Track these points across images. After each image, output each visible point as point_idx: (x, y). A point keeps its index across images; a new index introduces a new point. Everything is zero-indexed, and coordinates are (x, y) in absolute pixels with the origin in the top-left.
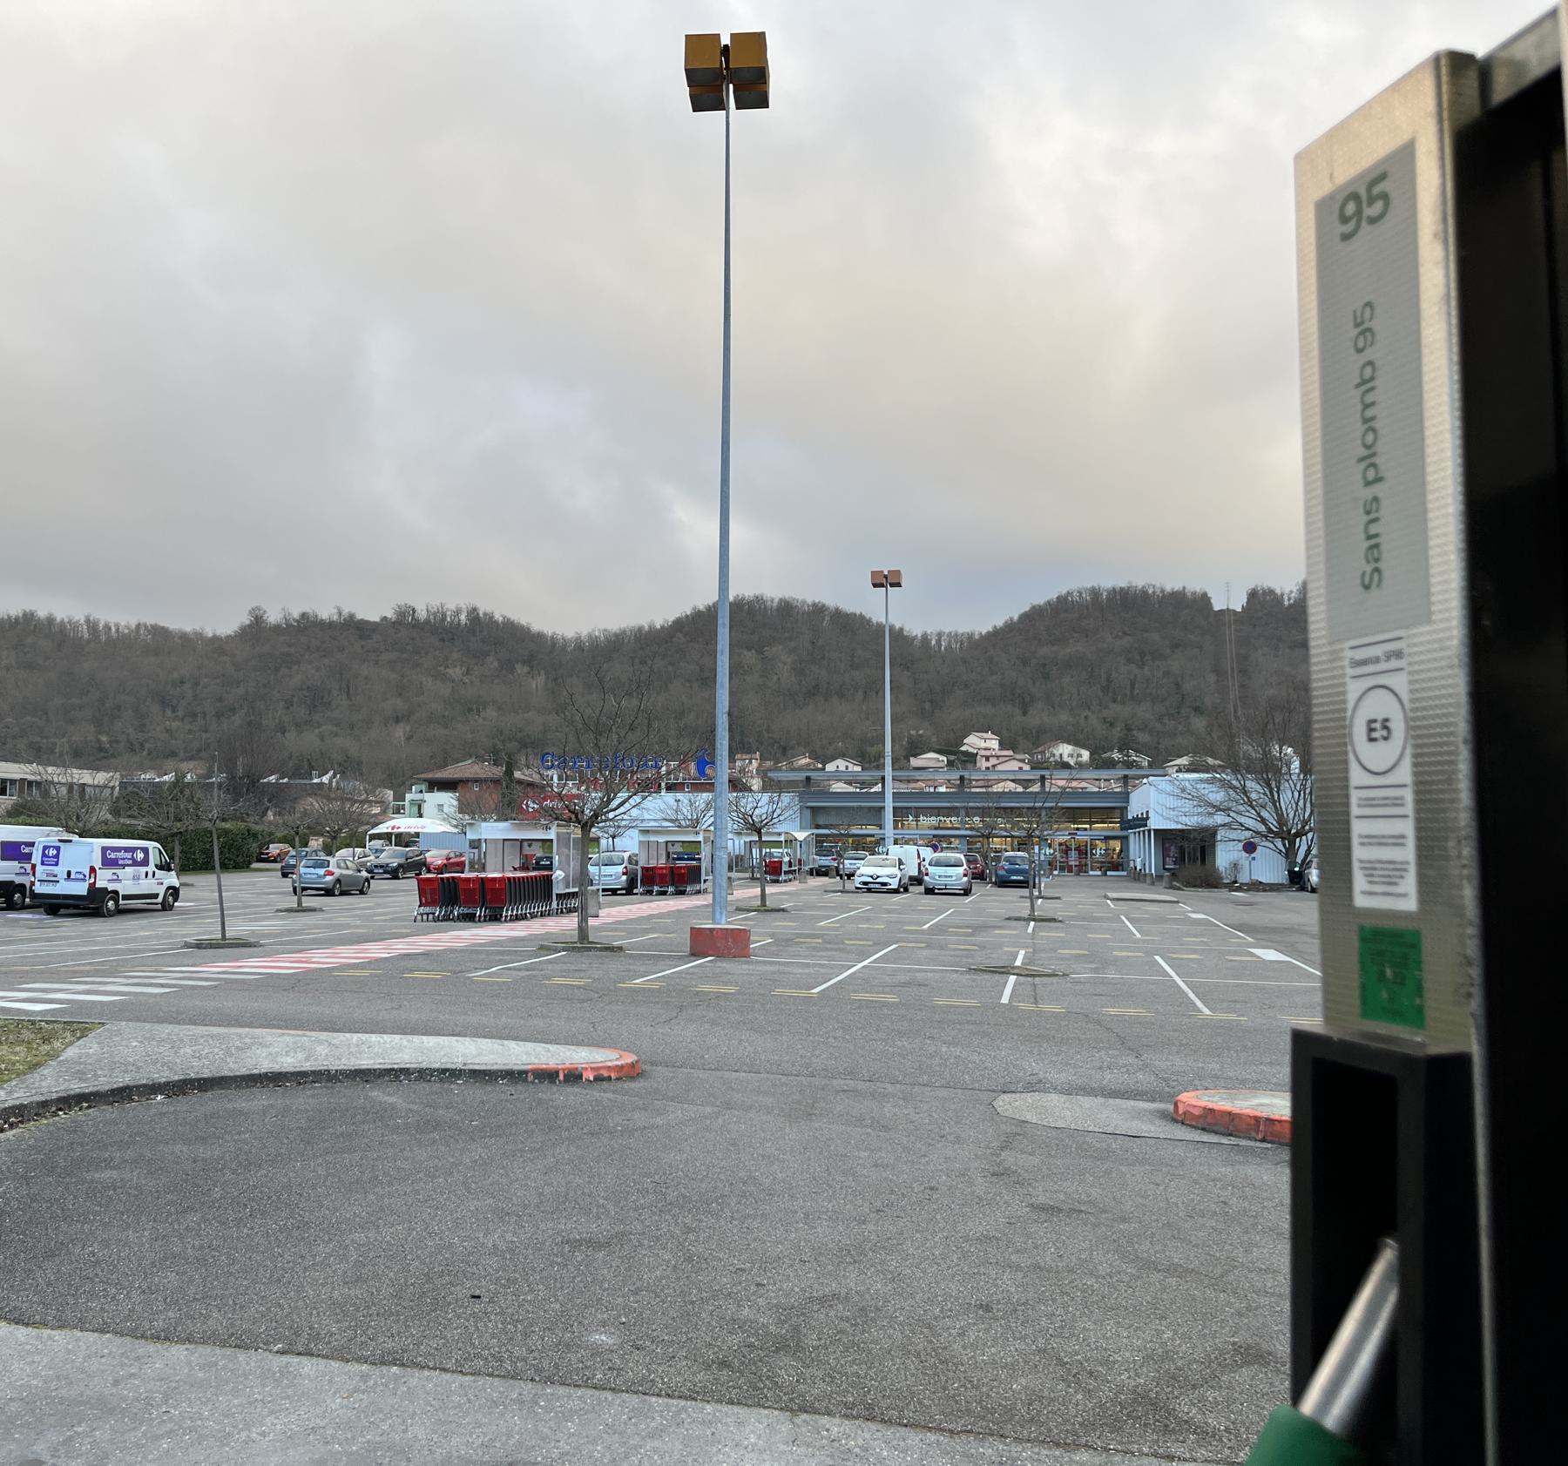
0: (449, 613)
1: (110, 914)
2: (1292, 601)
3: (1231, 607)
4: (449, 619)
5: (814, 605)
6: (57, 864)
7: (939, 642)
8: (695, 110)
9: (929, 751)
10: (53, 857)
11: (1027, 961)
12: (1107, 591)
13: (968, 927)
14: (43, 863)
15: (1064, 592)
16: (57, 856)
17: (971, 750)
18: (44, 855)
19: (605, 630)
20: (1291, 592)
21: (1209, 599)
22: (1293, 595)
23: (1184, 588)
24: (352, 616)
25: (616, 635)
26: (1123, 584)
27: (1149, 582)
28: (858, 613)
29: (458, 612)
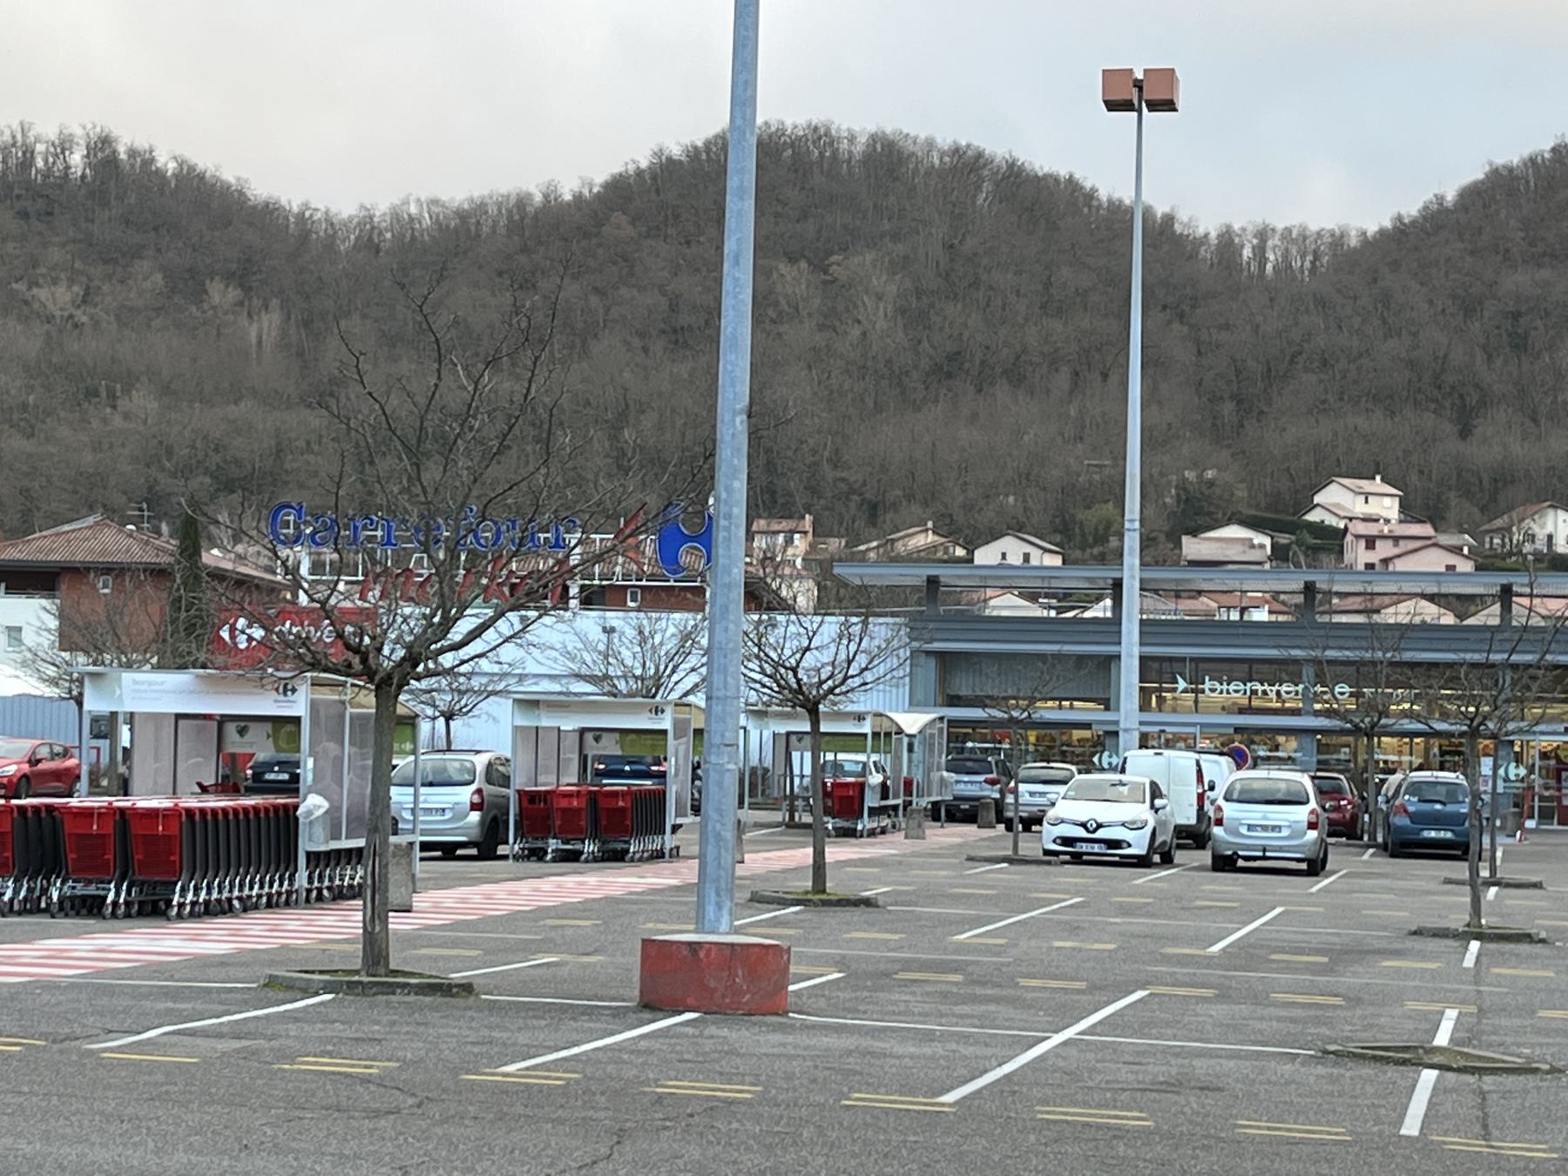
4: (40, 163)
5: (956, 151)
19: (435, 202)
29: (64, 145)
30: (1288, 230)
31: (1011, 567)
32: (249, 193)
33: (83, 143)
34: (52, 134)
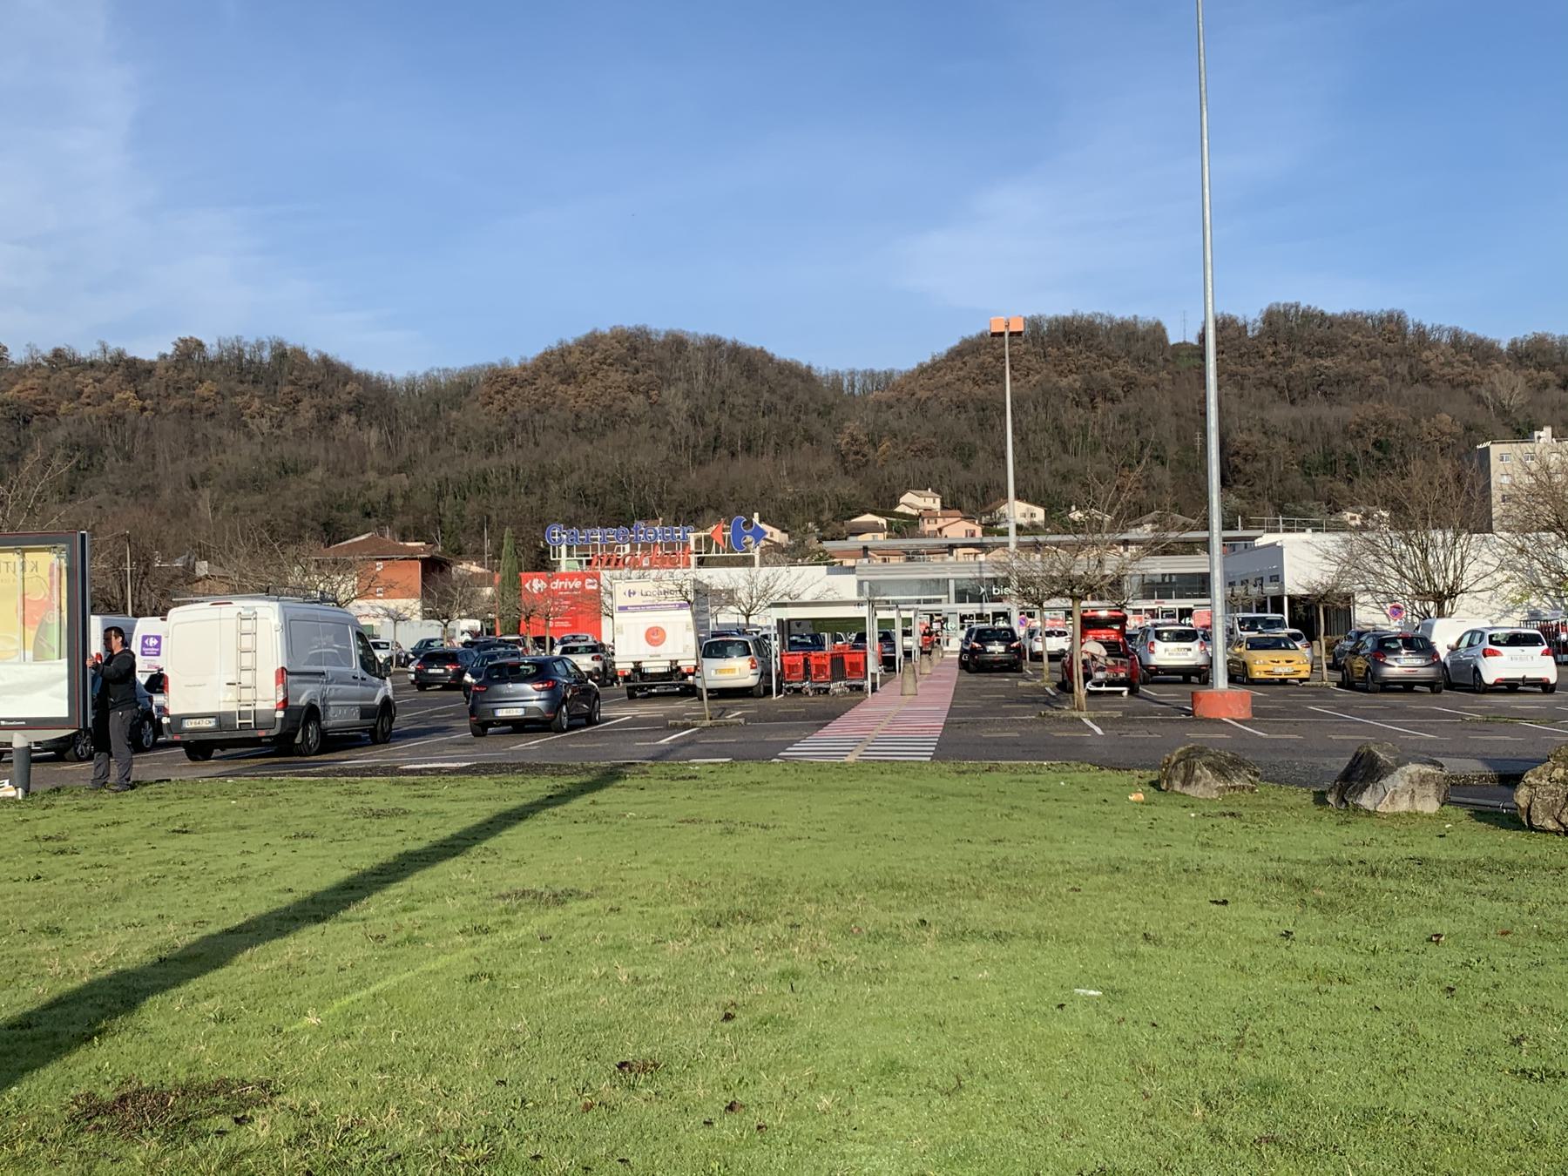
0: (247, 349)
1: (1283, 649)
2: (1256, 332)
3: (1188, 340)
4: (248, 357)
5: (708, 339)
6: (158, 654)
9: (865, 513)
10: (155, 647)
12: (1050, 322)
13: (1417, 691)
14: (143, 654)
16: (158, 646)
17: (908, 511)
18: (144, 645)
19: (446, 370)
20: (1255, 321)
21: (1164, 331)
22: (1258, 324)
23: (1135, 317)
24: (120, 354)
26: (1068, 313)
27: (1096, 311)
29: (260, 346)
30: (865, 372)
31: (960, 563)
32: (352, 368)
33: (268, 345)
34: (252, 341)
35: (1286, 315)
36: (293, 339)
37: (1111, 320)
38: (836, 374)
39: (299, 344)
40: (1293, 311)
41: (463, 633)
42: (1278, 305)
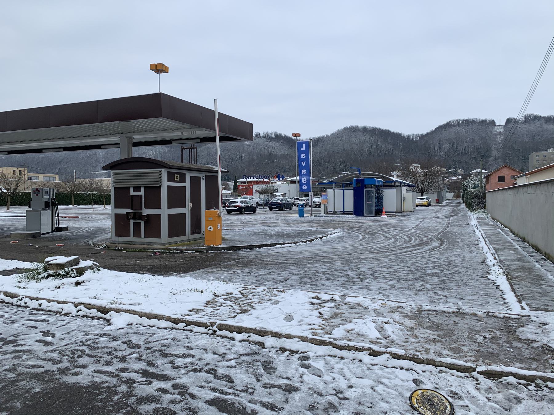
5: (373, 128)
7: (413, 137)
8: (252, 124)
11: (35, 172)
12: (489, 120)
15: (449, 121)
25: (317, 139)
28: (387, 129)
29: (272, 134)
34: (270, 132)
35: (530, 116)
36: (279, 132)
37: (479, 120)
38: (409, 135)
39: (280, 133)
40: (532, 116)
41: (522, 308)
42: (528, 114)
